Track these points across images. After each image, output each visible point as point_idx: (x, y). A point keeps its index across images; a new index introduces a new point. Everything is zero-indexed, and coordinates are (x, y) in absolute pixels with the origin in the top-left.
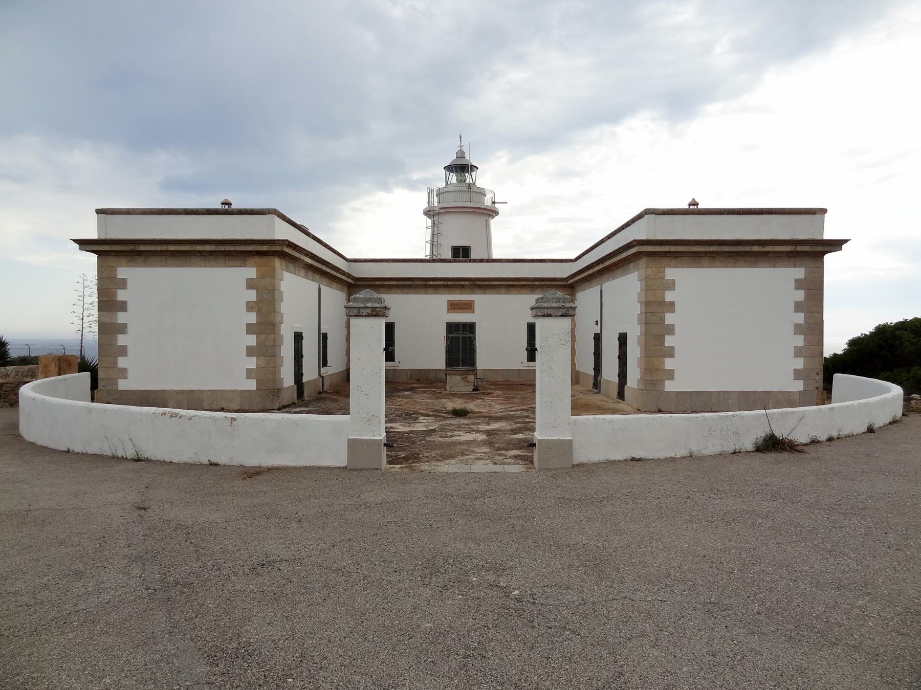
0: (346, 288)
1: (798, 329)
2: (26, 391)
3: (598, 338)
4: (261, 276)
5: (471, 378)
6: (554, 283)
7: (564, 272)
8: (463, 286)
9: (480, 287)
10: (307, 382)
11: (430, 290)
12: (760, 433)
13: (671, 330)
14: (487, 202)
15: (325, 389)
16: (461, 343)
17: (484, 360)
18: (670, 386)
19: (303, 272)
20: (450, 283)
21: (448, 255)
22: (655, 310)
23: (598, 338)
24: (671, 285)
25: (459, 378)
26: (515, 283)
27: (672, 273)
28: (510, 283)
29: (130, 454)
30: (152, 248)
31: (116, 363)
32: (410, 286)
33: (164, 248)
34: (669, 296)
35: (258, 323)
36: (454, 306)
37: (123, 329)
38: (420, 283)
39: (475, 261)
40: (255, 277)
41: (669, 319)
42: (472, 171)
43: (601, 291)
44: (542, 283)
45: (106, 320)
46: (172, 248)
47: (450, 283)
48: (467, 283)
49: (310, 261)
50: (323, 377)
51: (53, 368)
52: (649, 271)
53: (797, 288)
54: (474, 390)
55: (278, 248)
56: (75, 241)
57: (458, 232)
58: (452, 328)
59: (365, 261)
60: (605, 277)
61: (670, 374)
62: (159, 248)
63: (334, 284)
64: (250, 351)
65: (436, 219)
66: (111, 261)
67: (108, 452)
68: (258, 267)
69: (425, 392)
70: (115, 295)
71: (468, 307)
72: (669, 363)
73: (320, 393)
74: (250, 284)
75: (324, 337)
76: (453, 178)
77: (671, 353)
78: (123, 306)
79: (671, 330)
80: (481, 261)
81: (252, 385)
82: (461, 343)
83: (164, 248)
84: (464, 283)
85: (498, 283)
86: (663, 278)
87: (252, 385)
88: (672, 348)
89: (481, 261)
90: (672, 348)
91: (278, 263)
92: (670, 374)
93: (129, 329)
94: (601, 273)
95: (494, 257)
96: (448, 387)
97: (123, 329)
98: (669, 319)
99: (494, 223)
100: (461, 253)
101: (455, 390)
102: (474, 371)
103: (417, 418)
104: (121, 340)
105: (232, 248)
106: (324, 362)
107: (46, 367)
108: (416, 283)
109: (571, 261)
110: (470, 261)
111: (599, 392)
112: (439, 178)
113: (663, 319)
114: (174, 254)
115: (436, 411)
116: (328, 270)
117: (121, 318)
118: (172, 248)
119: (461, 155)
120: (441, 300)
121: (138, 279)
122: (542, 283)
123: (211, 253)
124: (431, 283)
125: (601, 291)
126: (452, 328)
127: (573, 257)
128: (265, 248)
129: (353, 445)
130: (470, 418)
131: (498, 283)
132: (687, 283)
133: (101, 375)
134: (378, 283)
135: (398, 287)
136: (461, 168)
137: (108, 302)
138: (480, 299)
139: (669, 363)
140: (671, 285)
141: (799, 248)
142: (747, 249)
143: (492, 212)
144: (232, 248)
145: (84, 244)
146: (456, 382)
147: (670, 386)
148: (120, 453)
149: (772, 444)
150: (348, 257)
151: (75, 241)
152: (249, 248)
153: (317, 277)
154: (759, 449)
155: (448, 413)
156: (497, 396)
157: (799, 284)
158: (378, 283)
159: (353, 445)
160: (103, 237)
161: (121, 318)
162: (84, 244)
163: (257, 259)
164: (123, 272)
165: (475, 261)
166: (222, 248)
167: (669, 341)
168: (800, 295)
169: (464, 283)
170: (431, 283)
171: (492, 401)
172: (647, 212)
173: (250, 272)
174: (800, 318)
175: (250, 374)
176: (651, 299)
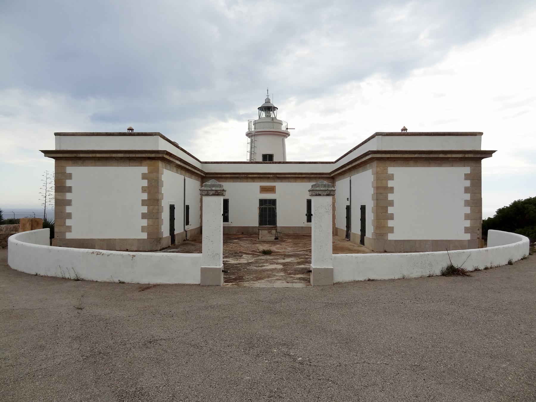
0: (200, 179)
1: (467, 203)
2: (12, 239)
3: (348, 208)
4: (150, 172)
5: (274, 232)
6: (323, 176)
7: (329, 169)
8: (269, 177)
9: (279, 178)
10: (177, 234)
11: (250, 180)
12: (444, 265)
13: (391, 203)
14: (283, 128)
15: (188, 238)
16: (268, 211)
17: (282, 221)
18: (391, 237)
19: (175, 169)
20: (261, 176)
21: (260, 159)
22: (382, 192)
23: (348, 208)
24: (391, 177)
25: (266, 232)
26: (300, 176)
27: (392, 170)
28: (297, 176)
29: (73, 276)
30: (87, 155)
31: (65, 223)
32: (238, 178)
33: (94, 155)
34: (390, 184)
35: (149, 199)
36: (264, 190)
37: (69, 203)
38: (243, 176)
39: (276, 163)
40: (147, 172)
41: (390, 197)
42: (274, 110)
43: (350, 181)
44: (315, 176)
45: (59, 198)
46: (98, 155)
47: (261, 176)
48: (271, 176)
49: (179, 163)
50: (186, 231)
51: (28, 226)
52: (379, 169)
53: (466, 179)
54: (275, 239)
55: (160, 155)
56: (42, 151)
57: (266, 146)
58: (262, 202)
59: (212, 163)
60: (353, 172)
61: (391, 230)
62: (91, 155)
63: (193, 177)
64: (144, 216)
65: (253, 138)
66: (63, 163)
67: (60, 275)
68: (149, 166)
69: (247, 240)
70: (65, 183)
71: (272, 190)
72: (390, 223)
73: (184, 240)
74: (144, 177)
75: (188, 207)
76: (263, 114)
77: (391, 217)
78: (69, 189)
79: (391, 203)
80: (280, 163)
81: (144, 236)
82: (268, 211)
83: (94, 155)
84: (269, 176)
85: (289, 176)
86: (387, 173)
87: (144, 236)
88: (392, 214)
89: (280, 163)
90: (392, 214)
91: (160, 164)
92: (391, 230)
93: (73, 203)
94: (350, 170)
95: (287, 161)
96: (260, 237)
97: (69, 203)
98: (390, 197)
99: (287, 140)
100: (268, 158)
101: (264, 239)
102: (275, 228)
103: (242, 256)
104: (68, 209)
105: (134, 155)
106: (187, 222)
107: (24, 225)
108: (241, 176)
109: (332, 163)
110: (273, 163)
111: (350, 240)
112: (255, 115)
113: (387, 197)
114: (100, 159)
115: (253, 251)
116: (190, 168)
117: (68, 196)
118: (98, 155)
119: (268, 101)
120: (255, 187)
121: (79, 173)
122: (315, 176)
123: (121, 158)
124: (250, 176)
125: (350, 181)
126: (262, 202)
127: (334, 160)
128: (153, 155)
129: (204, 271)
130: (273, 255)
131: (289, 176)
132: (401, 176)
133: (56, 230)
134: (219, 176)
135: (231, 178)
136: (268, 108)
137: (61, 187)
138: (279, 185)
139: (390, 223)
140: (391, 177)
141: (467, 156)
142: (436, 156)
143: (286, 134)
144: (134, 155)
145: (47, 153)
146: (264, 234)
147: (391, 237)
148: (67, 276)
149: (452, 271)
150: (201, 160)
151: (42, 151)
152: (144, 155)
153: (184, 172)
154: (444, 274)
155: (260, 252)
156: (289, 243)
157: (467, 177)
158: (219, 176)
159: (204, 271)
160: (58, 149)
161: (68, 196)
162: (47, 153)
163: (148, 162)
164: (70, 169)
165: (276, 163)
166: (128, 155)
167: (390, 210)
168: (468, 183)
169: (269, 176)
170: (250, 176)
171: (286, 245)
172: (377, 134)
173: (144, 169)
174: (468, 197)
175: (143, 229)
176: (380, 185)
